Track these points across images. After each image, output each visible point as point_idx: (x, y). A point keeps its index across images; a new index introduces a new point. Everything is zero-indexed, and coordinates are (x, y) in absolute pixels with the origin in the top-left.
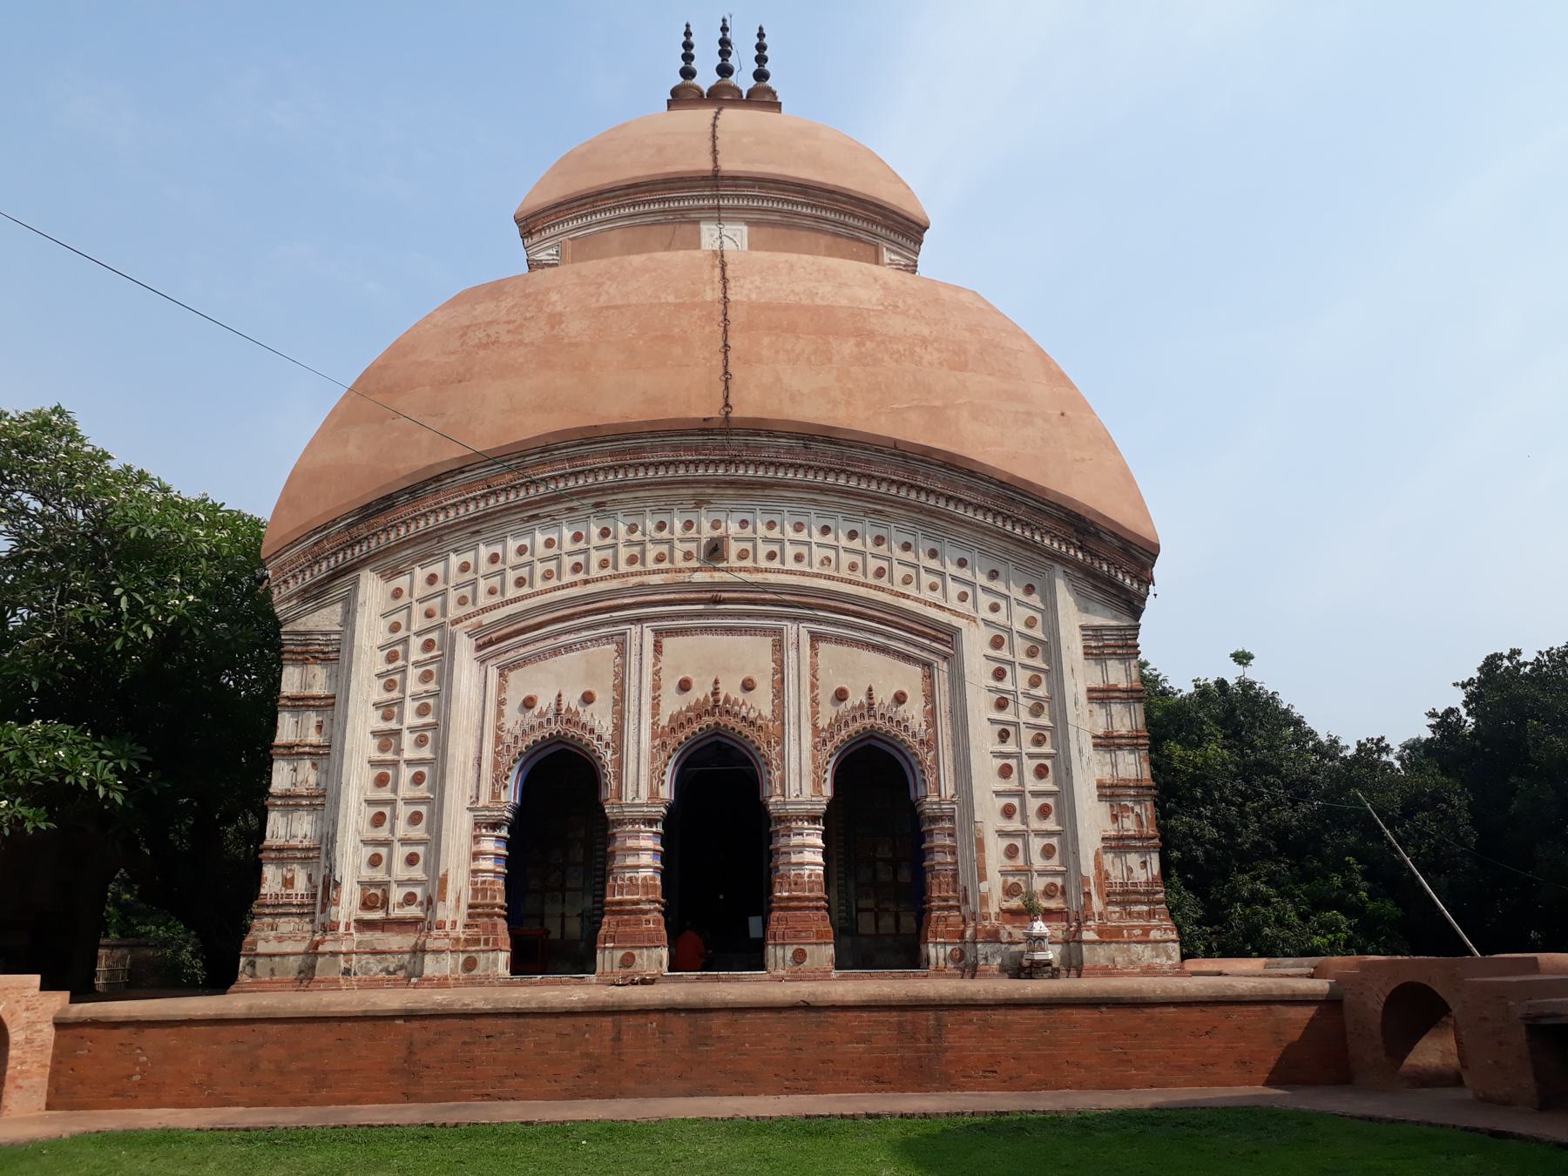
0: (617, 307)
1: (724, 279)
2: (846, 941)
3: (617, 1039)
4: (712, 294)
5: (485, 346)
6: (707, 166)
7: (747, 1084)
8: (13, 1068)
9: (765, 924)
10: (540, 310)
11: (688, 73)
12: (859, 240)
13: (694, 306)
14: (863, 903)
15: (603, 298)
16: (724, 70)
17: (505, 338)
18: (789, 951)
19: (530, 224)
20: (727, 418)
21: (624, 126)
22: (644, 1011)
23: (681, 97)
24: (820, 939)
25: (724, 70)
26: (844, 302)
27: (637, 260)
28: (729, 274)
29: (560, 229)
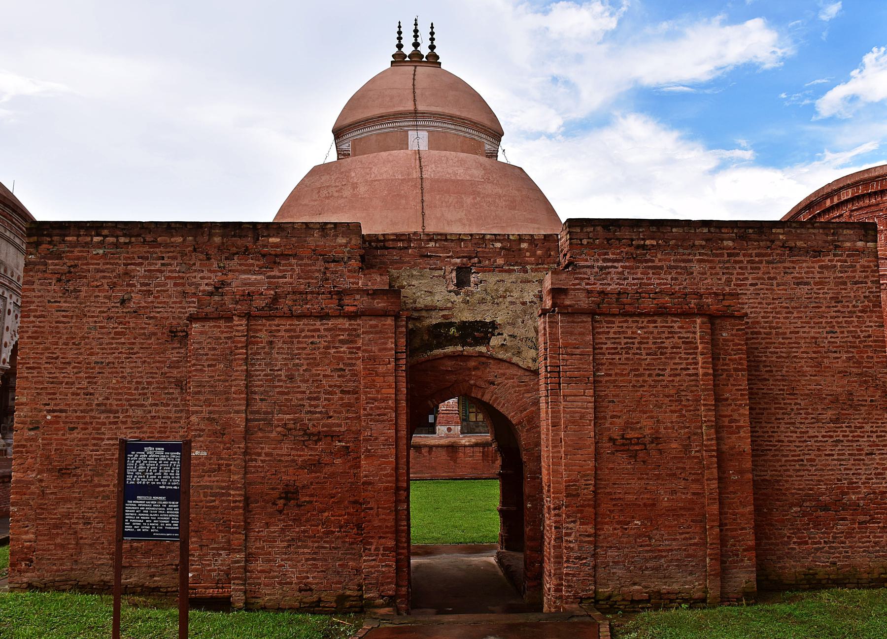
0: (379, 180)
1: (414, 75)
2: (465, 423)
4: (416, 174)
5: (328, 198)
11: (400, 46)
13: (409, 180)
14: (471, 410)
15: (373, 176)
16: (416, 45)
17: (336, 194)
20: (416, 66)
23: (399, 59)
24: (457, 424)
25: (416, 45)
26: (468, 178)
28: (422, 164)
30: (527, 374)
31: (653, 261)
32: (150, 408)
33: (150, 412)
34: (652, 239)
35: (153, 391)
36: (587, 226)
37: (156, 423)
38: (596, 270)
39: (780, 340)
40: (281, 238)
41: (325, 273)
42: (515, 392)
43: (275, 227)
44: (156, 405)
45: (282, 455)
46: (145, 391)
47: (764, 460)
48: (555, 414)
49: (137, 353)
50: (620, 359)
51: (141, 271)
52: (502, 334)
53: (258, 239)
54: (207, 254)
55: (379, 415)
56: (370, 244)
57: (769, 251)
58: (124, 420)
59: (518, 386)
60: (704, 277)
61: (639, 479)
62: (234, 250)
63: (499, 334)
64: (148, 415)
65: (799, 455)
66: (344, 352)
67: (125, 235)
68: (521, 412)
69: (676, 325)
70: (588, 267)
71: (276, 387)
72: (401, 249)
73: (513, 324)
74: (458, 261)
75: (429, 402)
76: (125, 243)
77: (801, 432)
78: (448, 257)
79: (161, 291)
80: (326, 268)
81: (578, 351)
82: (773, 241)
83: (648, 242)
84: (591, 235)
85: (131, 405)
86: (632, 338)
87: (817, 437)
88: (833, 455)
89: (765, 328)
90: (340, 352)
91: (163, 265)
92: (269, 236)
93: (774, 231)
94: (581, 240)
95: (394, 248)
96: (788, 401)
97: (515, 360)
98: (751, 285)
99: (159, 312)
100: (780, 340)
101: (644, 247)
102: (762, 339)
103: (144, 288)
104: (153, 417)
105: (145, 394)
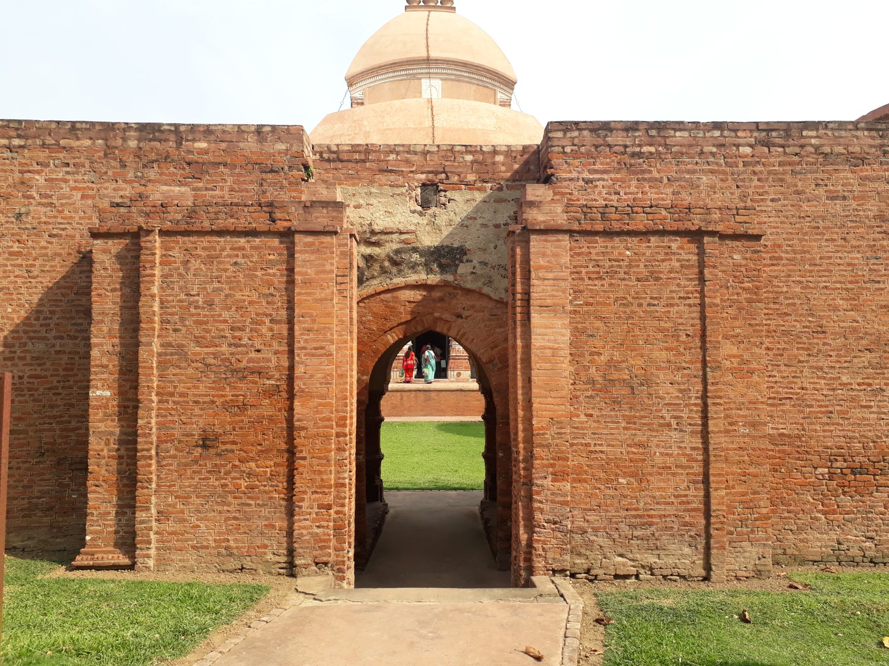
0: (391, 129)
3: (402, 399)
4: (428, 123)
6: (424, 54)
7: (443, 413)
8: (3, 455)
9: (447, 364)
10: (360, 130)
12: (487, 87)
18: (455, 373)
19: (351, 82)
21: (386, 26)
22: (410, 391)
27: (397, 103)
29: (364, 83)
30: (499, 306)
31: (650, 172)
32: (54, 342)
33: (54, 346)
34: (651, 145)
35: (57, 322)
36: (571, 130)
37: (61, 359)
38: (581, 183)
39: (807, 267)
40: (209, 142)
41: (261, 185)
42: (485, 326)
43: (201, 129)
44: (62, 338)
45: (200, 395)
46: (48, 321)
47: (783, 411)
48: (351, 312)
49: (38, 276)
50: (603, 285)
51: (40, 179)
52: (471, 261)
53: (181, 144)
54: (121, 161)
55: (316, 349)
56: (321, 156)
57: (796, 158)
58: (22, 355)
59: (489, 320)
60: (711, 193)
61: (625, 428)
62: (153, 156)
63: (468, 261)
64: (52, 350)
65: (827, 406)
66: (274, 275)
67: (19, 137)
68: (492, 348)
69: (674, 246)
70: (571, 180)
71: (193, 315)
72: (357, 162)
73: (484, 250)
74: (423, 176)
75: (389, 337)
76: (20, 147)
77: (831, 379)
78: (412, 172)
79: (66, 204)
80: (263, 179)
81: (551, 275)
82: (802, 146)
83: (645, 149)
84: (576, 141)
85: (31, 338)
86: (618, 261)
87: (851, 384)
88: (871, 407)
89: (788, 253)
90: (269, 275)
91: (68, 173)
92: (194, 140)
93: (804, 133)
94: (563, 147)
95: (349, 161)
96: (815, 341)
97: (486, 290)
98: (772, 200)
99: (63, 229)
100: (807, 267)
101: (639, 155)
102: (783, 265)
103: (44, 201)
104: (58, 352)
105: (49, 325)
